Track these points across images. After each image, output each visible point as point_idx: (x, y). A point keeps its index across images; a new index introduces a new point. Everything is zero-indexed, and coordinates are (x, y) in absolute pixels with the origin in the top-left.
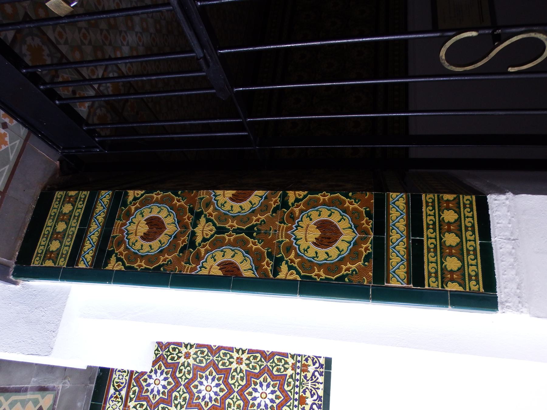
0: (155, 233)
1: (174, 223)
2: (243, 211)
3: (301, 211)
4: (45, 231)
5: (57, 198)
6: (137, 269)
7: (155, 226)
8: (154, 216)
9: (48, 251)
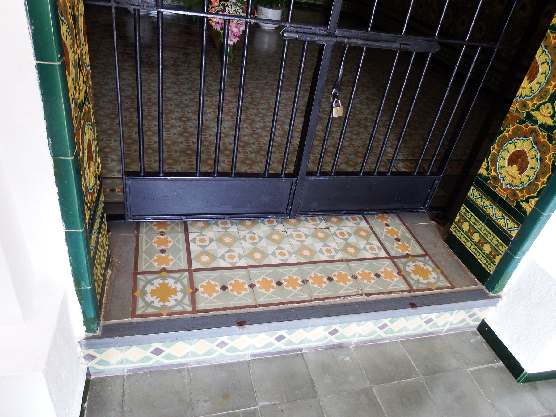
0: (523, 160)
1: (524, 141)
2: (547, 73)
3: (495, 171)
4: (472, 251)
5: (455, 231)
6: (544, 187)
7: (519, 159)
8: (509, 158)
9: (488, 256)
